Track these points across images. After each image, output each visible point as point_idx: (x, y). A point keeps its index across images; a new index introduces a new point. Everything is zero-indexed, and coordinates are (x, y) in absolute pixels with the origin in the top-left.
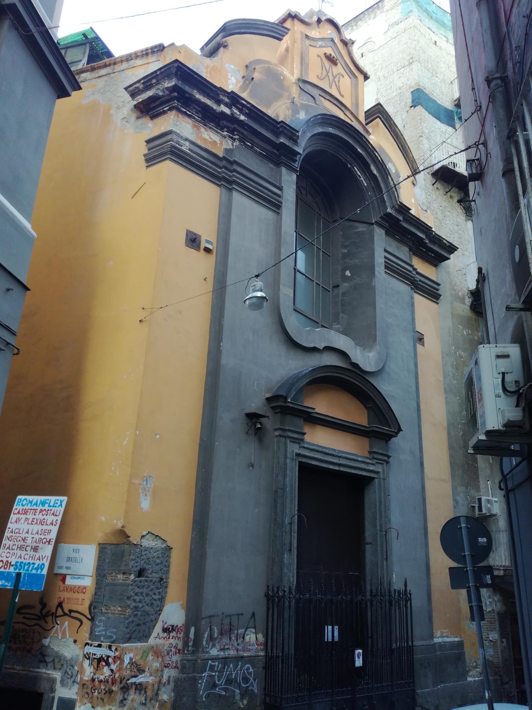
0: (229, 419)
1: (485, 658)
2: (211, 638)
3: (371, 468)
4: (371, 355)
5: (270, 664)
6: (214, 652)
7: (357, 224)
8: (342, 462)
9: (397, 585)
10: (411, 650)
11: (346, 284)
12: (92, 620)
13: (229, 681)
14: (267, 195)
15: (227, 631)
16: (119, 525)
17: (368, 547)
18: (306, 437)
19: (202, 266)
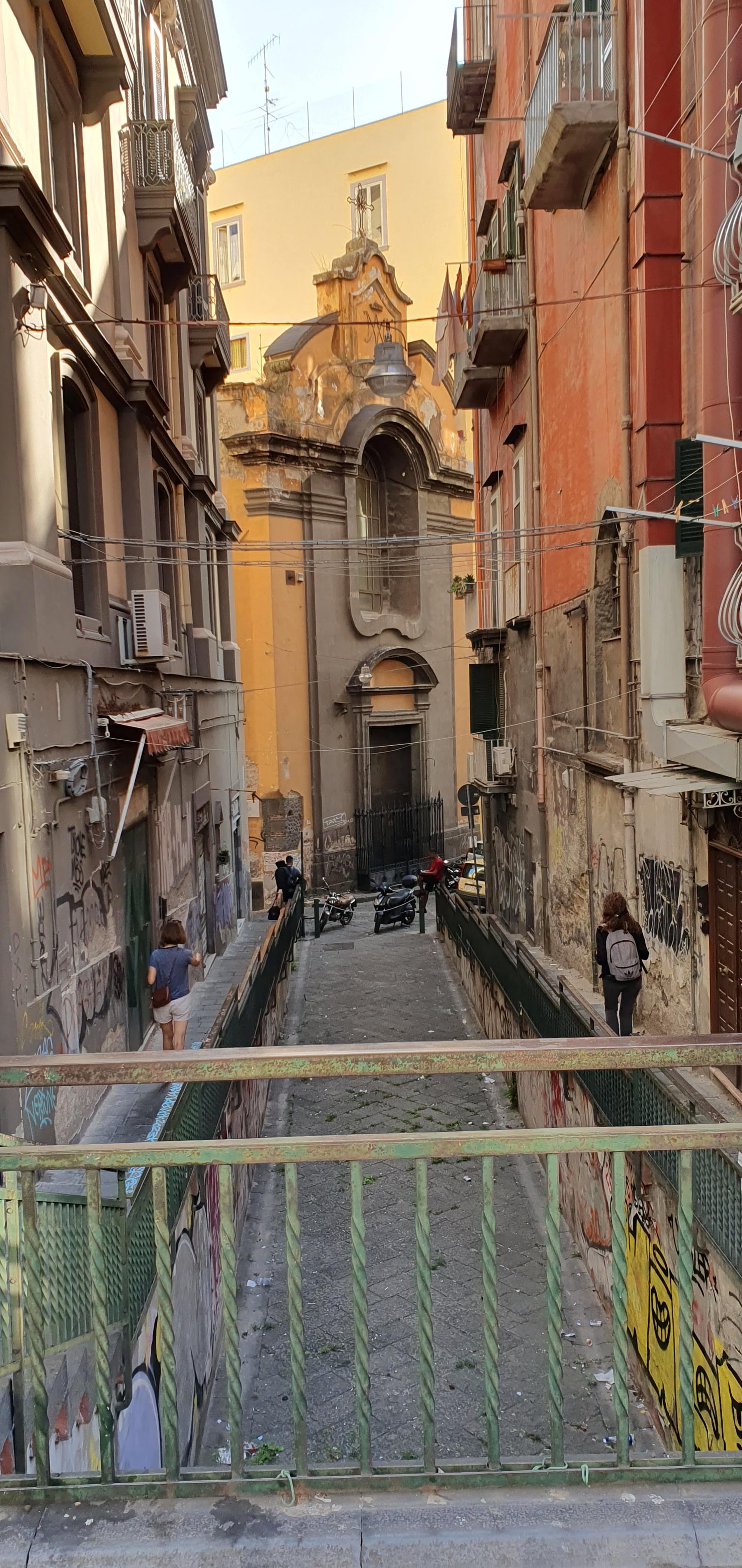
0: (325, 707)
1: (633, 801)
2: (328, 843)
3: (416, 717)
4: (415, 623)
5: (358, 853)
6: (330, 850)
7: (403, 487)
8: (397, 719)
9: (433, 796)
10: (442, 836)
11: (656, 1501)
12: (264, 841)
13: (339, 865)
14: (158, 63)
15: (336, 838)
16: (276, 789)
17: (413, 773)
18: (373, 710)
19: (297, 593)
